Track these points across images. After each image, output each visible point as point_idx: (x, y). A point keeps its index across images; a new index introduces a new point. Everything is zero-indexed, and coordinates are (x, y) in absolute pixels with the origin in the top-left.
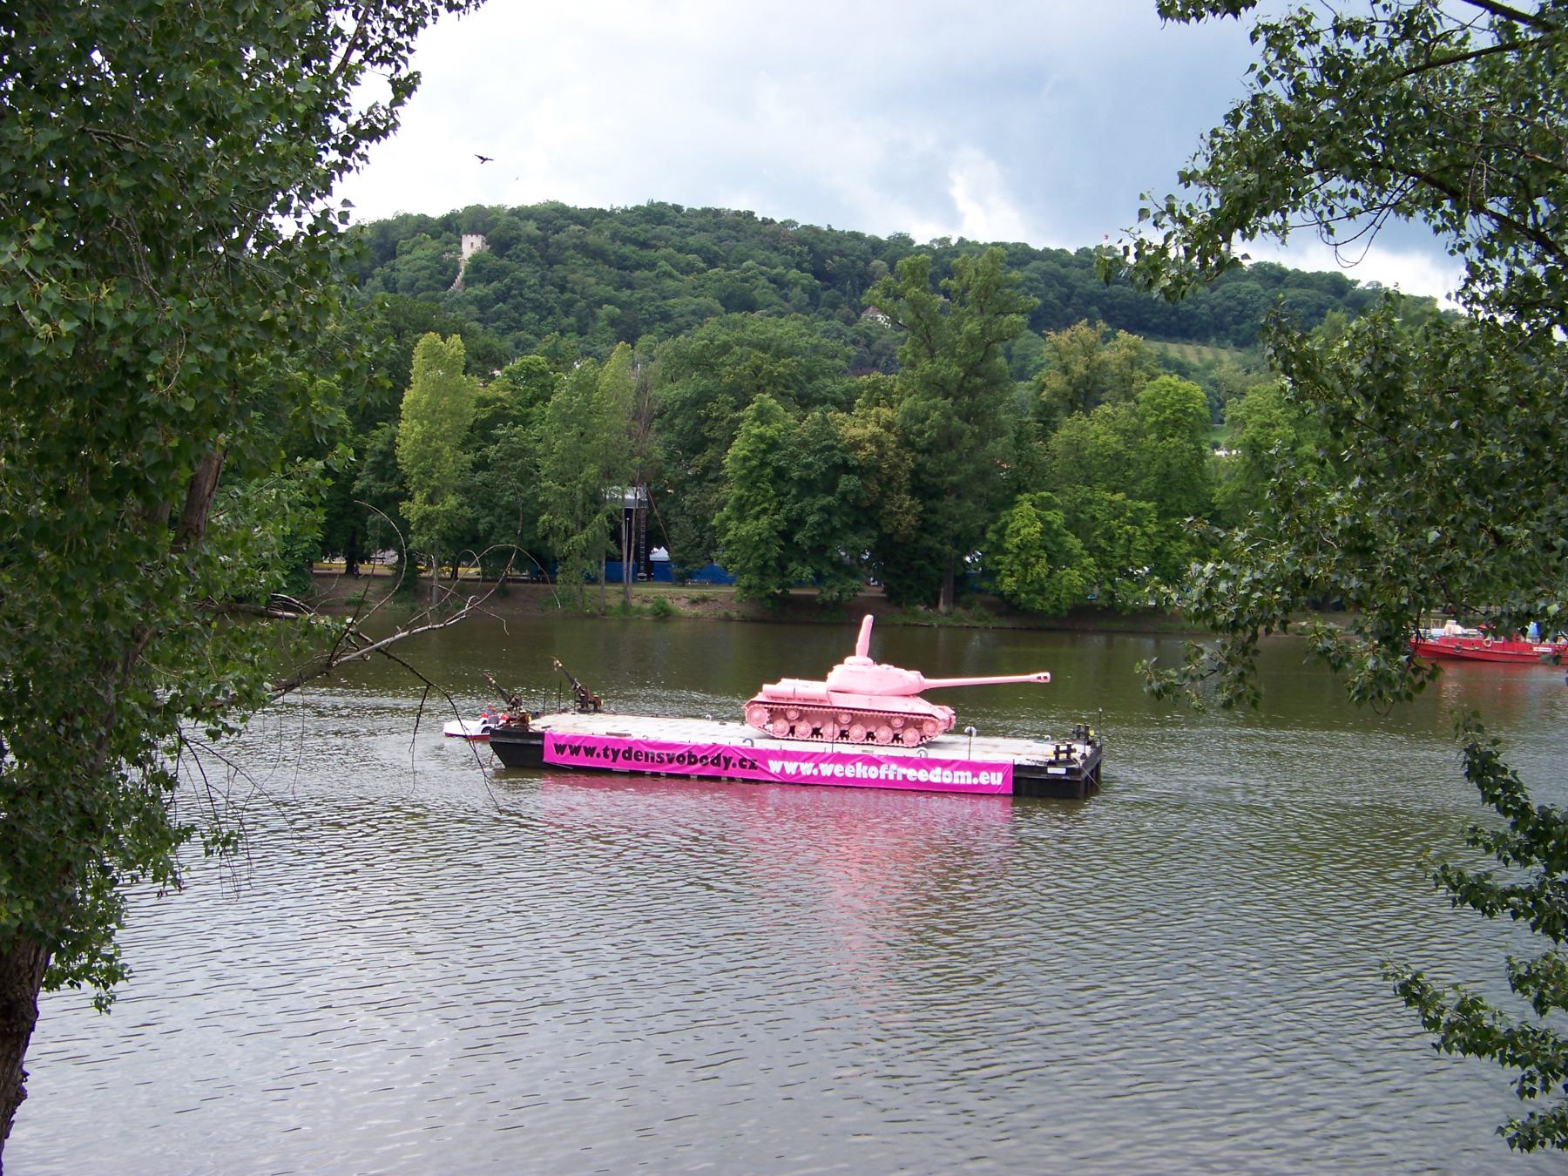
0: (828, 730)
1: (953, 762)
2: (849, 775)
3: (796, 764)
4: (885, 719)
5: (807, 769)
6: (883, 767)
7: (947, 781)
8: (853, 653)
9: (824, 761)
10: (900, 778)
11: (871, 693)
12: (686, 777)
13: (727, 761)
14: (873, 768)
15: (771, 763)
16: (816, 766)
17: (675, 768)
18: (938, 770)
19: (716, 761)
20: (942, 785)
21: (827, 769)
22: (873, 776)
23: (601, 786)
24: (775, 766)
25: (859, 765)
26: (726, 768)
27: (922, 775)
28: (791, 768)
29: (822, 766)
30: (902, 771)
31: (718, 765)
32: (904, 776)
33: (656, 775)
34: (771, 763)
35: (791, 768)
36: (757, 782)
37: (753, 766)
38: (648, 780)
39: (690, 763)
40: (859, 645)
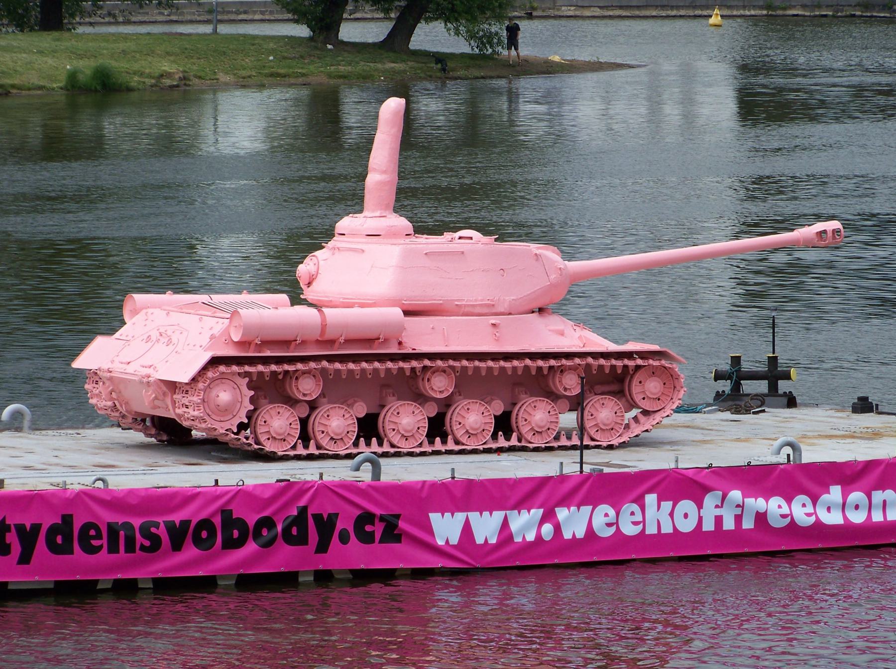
0: (472, 417)
1: (870, 465)
2: (629, 530)
3: (498, 516)
4: (534, 375)
5: (525, 524)
6: (710, 501)
7: (858, 518)
8: (354, 202)
9: (565, 501)
10: (748, 524)
11: (489, 310)
12: (208, 584)
13: (326, 526)
14: (687, 506)
15: (435, 518)
16: (549, 516)
17: (170, 564)
18: (835, 493)
19: (296, 532)
20: (848, 529)
21: (574, 522)
22: (687, 526)
23: (593, 569)
24: (446, 528)
25: (651, 499)
26: (322, 547)
27: (801, 511)
28: (486, 526)
29: (562, 514)
30: (775, 507)
31: (302, 540)
32: (761, 518)
33: (126, 589)
34: (435, 518)
35: (486, 526)
36: (387, 576)
37: (392, 533)
38: (106, 604)
39: (231, 544)
40: (373, 179)
